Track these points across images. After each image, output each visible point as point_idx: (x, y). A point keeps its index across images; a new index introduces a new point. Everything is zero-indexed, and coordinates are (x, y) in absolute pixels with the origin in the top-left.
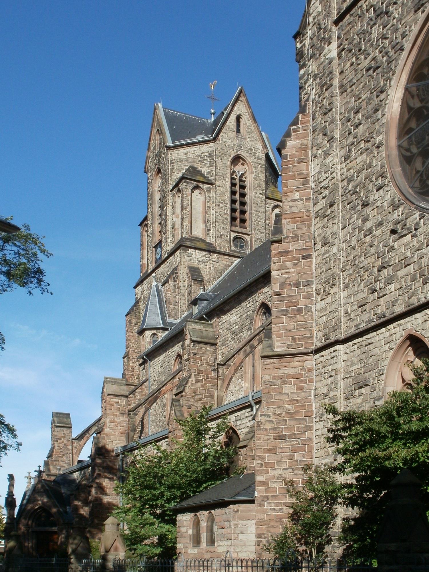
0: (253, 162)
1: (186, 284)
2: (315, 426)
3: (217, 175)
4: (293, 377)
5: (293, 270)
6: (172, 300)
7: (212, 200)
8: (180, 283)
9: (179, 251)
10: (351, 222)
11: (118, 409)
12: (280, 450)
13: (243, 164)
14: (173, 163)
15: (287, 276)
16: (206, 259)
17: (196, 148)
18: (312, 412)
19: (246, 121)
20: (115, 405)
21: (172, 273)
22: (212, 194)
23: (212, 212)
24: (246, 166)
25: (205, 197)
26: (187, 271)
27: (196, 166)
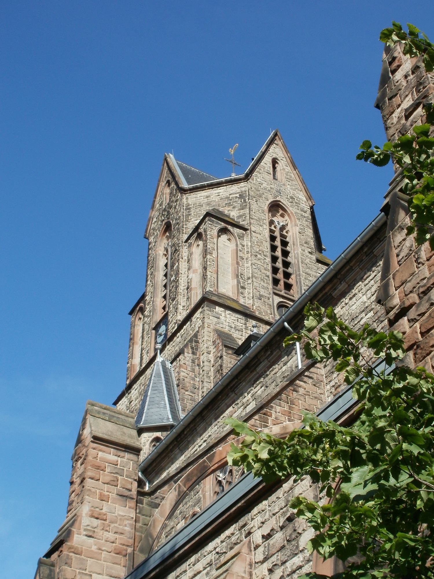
0: (296, 213)
1: (211, 357)
3: (252, 219)
6: (188, 382)
7: (246, 250)
8: (202, 358)
9: (200, 310)
11: (113, 483)
13: (282, 216)
14: (189, 209)
19: (283, 165)
20: (108, 470)
21: (191, 341)
22: (246, 241)
23: (246, 265)
24: (286, 217)
25: (237, 245)
26: (213, 336)
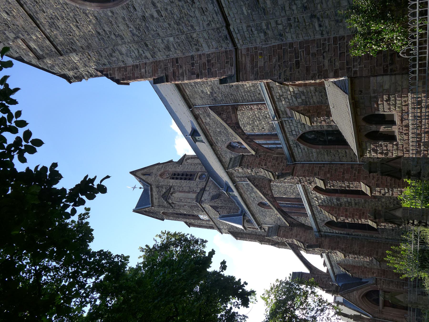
2: (290, 40)
4: (252, 61)
5: (184, 68)
6: (228, 210)
10: (155, 29)
11: (288, 232)
12: (308, 63)
15: (187, 71)
16: (208, 193)
17: (154, 194)
18: (278, 45)
27: (162, 194)
